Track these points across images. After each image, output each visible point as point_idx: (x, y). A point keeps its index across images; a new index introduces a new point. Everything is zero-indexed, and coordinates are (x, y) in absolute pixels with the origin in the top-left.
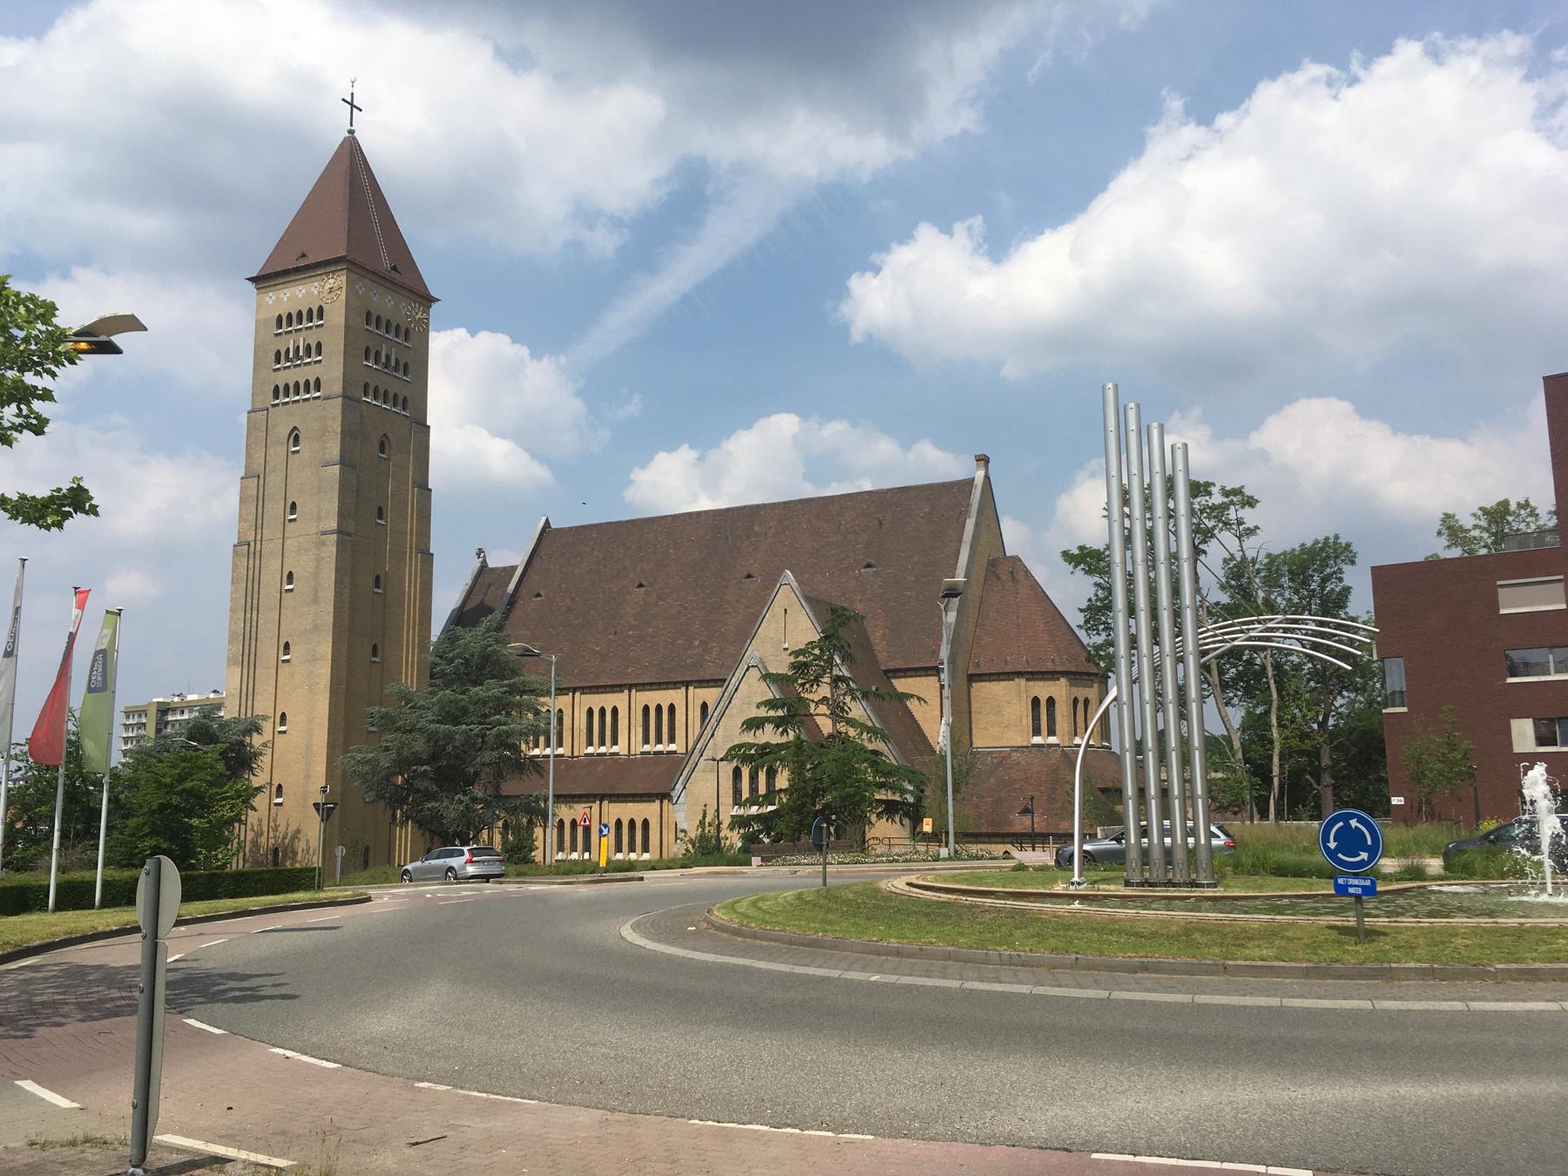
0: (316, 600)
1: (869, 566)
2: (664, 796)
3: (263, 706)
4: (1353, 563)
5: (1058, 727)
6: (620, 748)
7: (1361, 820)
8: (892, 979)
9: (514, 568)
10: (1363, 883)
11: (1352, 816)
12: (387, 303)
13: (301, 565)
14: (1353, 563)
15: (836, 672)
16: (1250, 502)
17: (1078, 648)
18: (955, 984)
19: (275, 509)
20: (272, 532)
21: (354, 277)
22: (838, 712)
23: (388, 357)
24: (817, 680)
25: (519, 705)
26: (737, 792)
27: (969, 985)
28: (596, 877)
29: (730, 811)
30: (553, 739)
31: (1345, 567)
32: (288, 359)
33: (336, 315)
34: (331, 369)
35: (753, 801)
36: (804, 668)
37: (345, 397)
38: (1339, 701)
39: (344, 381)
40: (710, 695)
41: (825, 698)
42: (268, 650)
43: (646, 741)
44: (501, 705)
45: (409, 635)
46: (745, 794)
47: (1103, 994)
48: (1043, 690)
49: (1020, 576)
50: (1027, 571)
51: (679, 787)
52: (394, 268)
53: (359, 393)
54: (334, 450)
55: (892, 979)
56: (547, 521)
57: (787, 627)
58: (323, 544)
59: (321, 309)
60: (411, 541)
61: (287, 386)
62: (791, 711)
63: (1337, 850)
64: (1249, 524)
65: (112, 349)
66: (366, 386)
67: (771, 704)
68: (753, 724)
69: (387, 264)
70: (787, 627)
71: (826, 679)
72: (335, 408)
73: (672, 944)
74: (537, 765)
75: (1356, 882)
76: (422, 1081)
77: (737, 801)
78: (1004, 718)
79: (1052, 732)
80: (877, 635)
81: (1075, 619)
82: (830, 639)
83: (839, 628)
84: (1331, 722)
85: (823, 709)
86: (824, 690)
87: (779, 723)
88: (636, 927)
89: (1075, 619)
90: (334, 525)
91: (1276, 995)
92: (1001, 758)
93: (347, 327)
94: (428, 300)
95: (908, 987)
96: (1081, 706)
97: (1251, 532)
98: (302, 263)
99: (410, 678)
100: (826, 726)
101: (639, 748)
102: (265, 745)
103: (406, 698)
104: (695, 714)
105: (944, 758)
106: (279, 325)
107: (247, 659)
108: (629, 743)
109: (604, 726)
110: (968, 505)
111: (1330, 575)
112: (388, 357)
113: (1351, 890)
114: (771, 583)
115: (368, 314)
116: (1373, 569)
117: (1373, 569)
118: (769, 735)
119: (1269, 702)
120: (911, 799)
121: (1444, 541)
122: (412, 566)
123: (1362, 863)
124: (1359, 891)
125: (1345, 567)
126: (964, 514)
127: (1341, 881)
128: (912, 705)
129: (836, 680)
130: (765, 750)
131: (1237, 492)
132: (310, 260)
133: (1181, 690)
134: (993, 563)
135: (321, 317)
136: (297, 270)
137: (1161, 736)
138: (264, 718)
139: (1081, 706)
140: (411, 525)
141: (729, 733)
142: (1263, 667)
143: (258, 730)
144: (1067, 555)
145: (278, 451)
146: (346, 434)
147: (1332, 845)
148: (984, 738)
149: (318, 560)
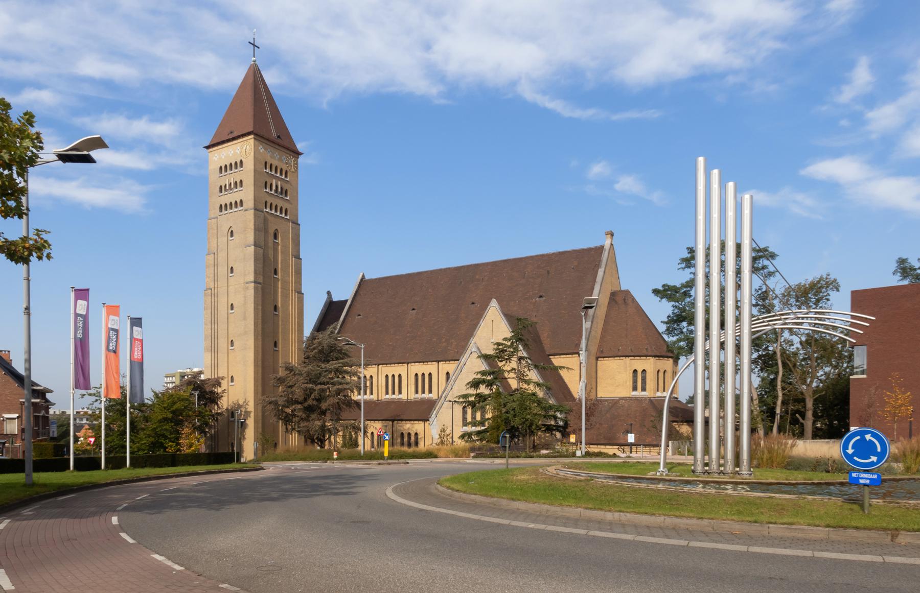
0: (245, 318)
1: (541, 297)
2: (426, 420)
3: (222, 372)
4: (838, 290)
5: (648, 387)
6: (403, 396)
7: (874, 435)
8: (542, 527)
9: (346, 301)
10: (871, 476)
11: (868, 432)
12: (276, 158)
13: (237, 300)
14: (838, 290)
15: (520, 354)
16: (773, 256)
17: (662, 342)
18: (582, 532)
19: (223, 270)
20: (222, 283)
21: (257, 143)
22: (521, 378)
23: (277, 187)
24: (509, 359)
25: (347, 372)
26: (464, 419)
27: (592, 533)
28: (381, 461)
29: (459, 430)
30: (368, 391)
31: (831, 293)
32: (226, 190)
33: (249, 165)
34: (247, 194)
35: (474, 424)
36: (501, 353)
37: (255, 209)
38: (821, 373)
39: (255, 200)
40: (449, 367)
41: (514, 369)
42: (223, 343)
43: (417, 392)
44: (338, 371)
45: (293, 336)
46: (469, 419)
47: (683, 543)
48: (640, 364)
49: (629, 301)
50: (633, 299)
51: (433, 416)
52: (279, 137)
53: (262, 206)
54: (251, 238)
55: (542, 527)
56: (363, 276)
57: (493, 328)
58: (247, 288)
59: (241, 161)
60: (292, 286)
61: (226, 205)
62: (495, 376)
63: (853, 454)
64: (772, 269)
65: (88, 159)
66: (266, 203)
67: (483, 373)
68: (475, 384)
69: (274, 134)
70: (493, 328)
71: (514, 359)
72: (250, 215)
73: (411, 500)
74: (358, 404)
75: (866, 476)
76: (223, 583)
77: (465, 424)
78: (616, 380)
79: (644, 389)
80: (544, 336)
81: (662, 328)
82: (518, 337)
83: (524, 333)
84: (814, 385)
85: (512, 375)
86: (513, 364)
87: (490, 384)
88: (395, 490)
89: (662, 328)
90: (252, 279)
91: (808, 549)
92: (614, 403)
93: (255, 171)
94: (297, 154)
95: (552, 532)
96: (661, 374)
97: (771, 274)
98: (231, 137)
99: (294, 359)
100: (514, 384)
101: (412, 396)
102: (223, 391)
103: (290, 369)
104: (443, 378)
105: (580, 400)
106: (221, 172)
107: (214, 349)
108: (408, 394)
109: (394, 383)
110: (600, 261)
111: (822, 298)
112: (277, 187)
113: (861, 481)
114: (484, 307)
115: (266, 163)
116: (853, 293)
117: (853, 293)
118: (483, 390)
119: (777, 373)
120: (561, 423)
121: (898, 276)
122: (293, 297)
123: (872, 464)
124: (868, 482)
125: (831, 293)
126: (598, 266)
127: (854, 475)
128: (563, 373)
129: (520, 359)
130: (482, 398)
131: (765, 250)
132: (235, 134)
133: (722, 366)
134: (614, 294)
135: (241, 166)
136: (228, 141)
137: (707, 394)
138: (223, 378)
139: (661, 374)
140: (292, 278)
141: (460, 387)
142: (775, 353)
143: (219, 385)
144: (656, 292)
145: (223, 240)
146: (257, 230)
147: (850, 451)
148: (605, 392)
149: (245, 297)
